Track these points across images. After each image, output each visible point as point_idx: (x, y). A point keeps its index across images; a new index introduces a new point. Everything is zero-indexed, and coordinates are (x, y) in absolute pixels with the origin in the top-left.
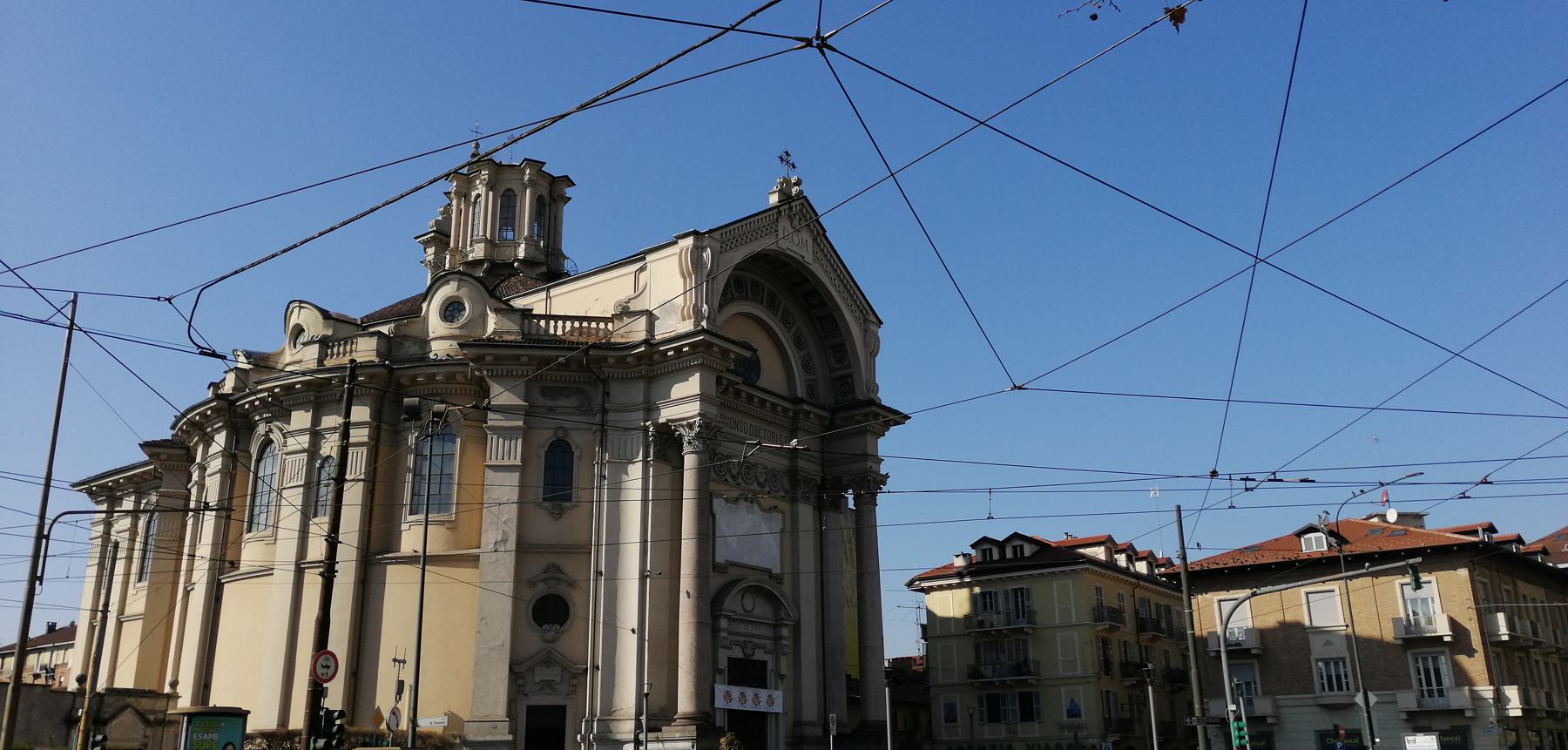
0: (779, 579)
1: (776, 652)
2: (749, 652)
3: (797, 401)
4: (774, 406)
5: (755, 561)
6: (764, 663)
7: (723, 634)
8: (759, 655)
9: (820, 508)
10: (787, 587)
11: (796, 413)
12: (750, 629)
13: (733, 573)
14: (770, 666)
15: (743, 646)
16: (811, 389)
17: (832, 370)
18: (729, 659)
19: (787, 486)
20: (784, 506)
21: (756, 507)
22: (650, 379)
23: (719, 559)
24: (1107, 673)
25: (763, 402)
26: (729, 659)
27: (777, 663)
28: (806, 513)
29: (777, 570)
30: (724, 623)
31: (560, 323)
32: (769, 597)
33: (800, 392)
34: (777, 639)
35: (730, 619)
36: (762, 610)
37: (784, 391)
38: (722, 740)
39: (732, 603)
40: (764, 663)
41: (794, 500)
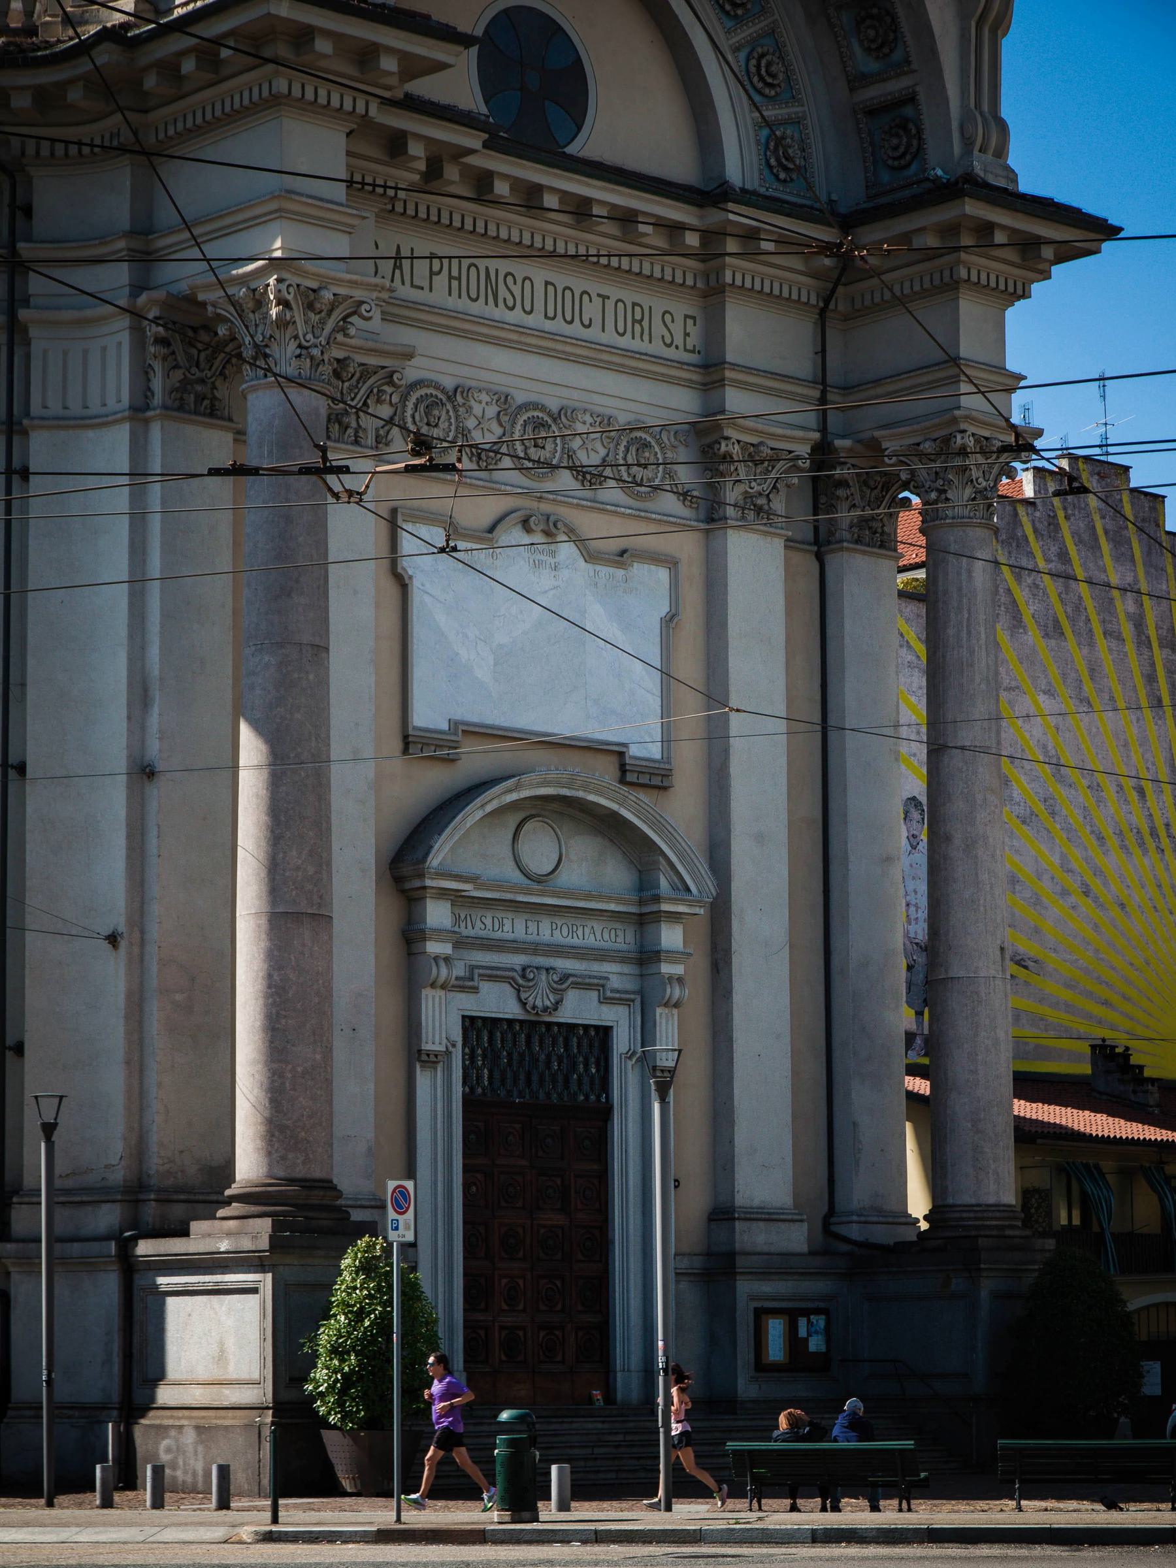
0: (652, 779)
1: (645, 1001)
2: (541, 997)
3: (711, 194)
4: (627, 219)
5: (567, 721)
6: (604, 1033)
7: (433, 948)
8: (579, 1009)
9: (820, 545)
10: (683, 807)
11: (710, 236)
12: (546, 931)
13: (476, 760)
14: (621, 1042)
15: (520, 981)
16: (778, 151)
17: (857, 81)
18: (470, 1023)
19: (685, 475)
20: (686, 546)
21: (567, 551)
22: (149, 156)
23: (428, 714)
24: (453, 761)
25: (580, 210)
26: (470, 1023)
27: (647, 1032)
28: (758, 566)
29: (646, 746)
30: (437, 914)
31: (657, 274)
32: (610, 827)
33: (738, 163)
34: (646, 957)
35: (457, 899)
36: (587, 868)
37: (679, 166)
38: (1136, 1302)
39: (469, 851)
40: (604, 1033)
41: (712, 517)
